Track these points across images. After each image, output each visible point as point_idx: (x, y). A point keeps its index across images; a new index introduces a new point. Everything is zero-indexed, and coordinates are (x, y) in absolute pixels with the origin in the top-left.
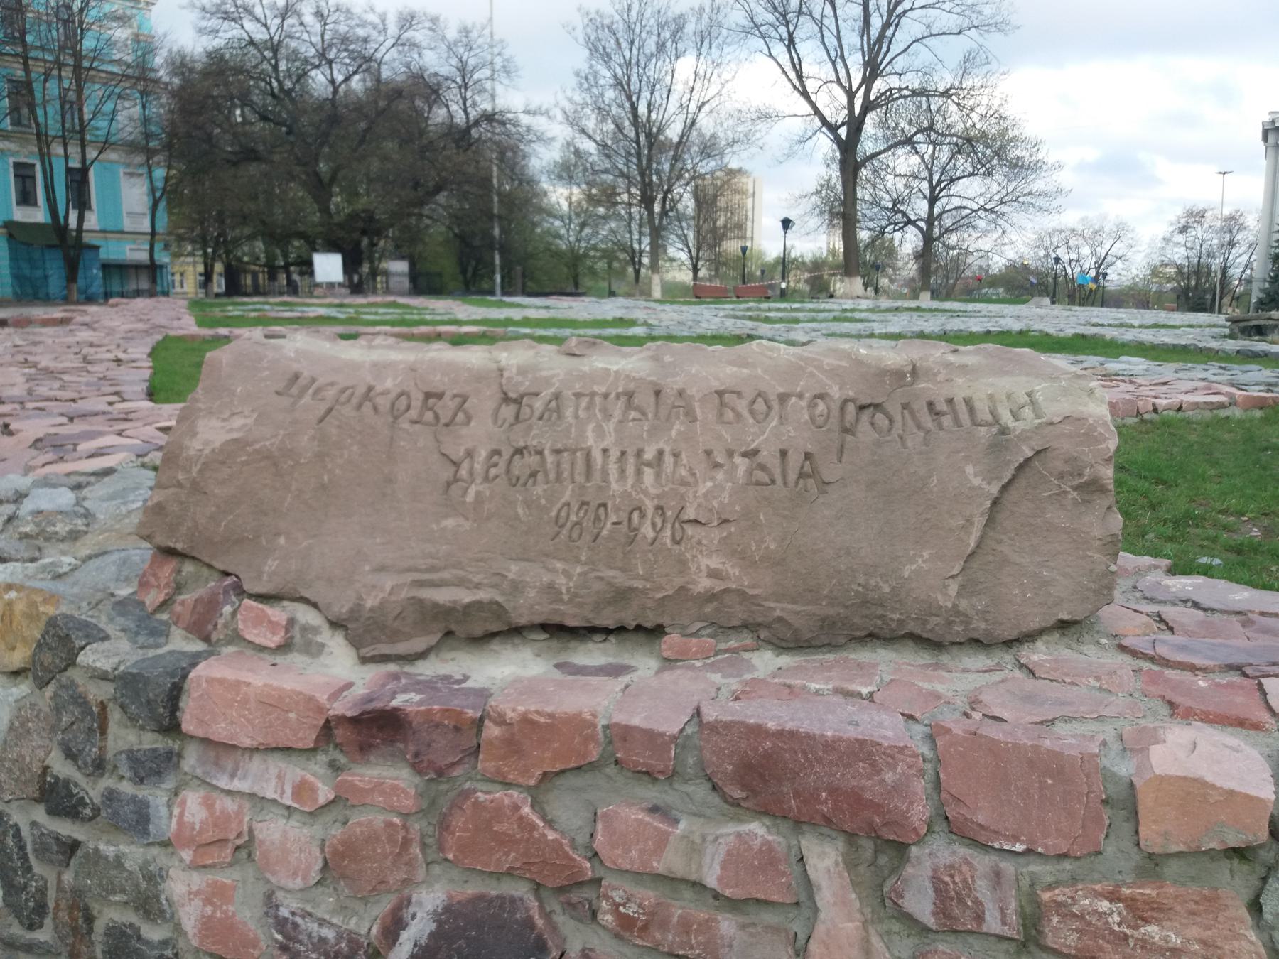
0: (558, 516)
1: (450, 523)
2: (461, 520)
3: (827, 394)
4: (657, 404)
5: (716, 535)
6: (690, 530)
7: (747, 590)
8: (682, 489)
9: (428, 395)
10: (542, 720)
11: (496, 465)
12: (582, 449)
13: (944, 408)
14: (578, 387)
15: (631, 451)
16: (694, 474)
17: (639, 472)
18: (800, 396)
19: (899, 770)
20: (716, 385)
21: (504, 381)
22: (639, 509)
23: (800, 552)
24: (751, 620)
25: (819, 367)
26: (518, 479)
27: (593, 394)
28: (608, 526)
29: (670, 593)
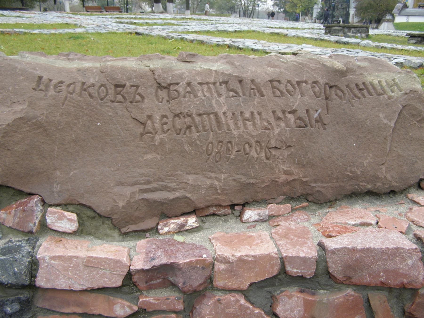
0: (207, 149)
1: (149, 156)
2: (155, 155)
3: (317, 81)
4: (242, 87)
5: (286, 153)
6: (274, 152)
7: (303, 179)
8: (267, 131)
9: (116, 86)
10: (250, 259)
11: (166, 123)
12: (212, 113)
13: (363, 87)
14: (199, 80)
15: (237, 113)
16: (270, 124)
17: (245, 125)
18: (306, 82)
19: (414, 259)
20: (268, 78)
21: (156, 77)
22: (248, 143)
23: (322, 159)
24: (304, 193)
25: (309, 68)
26: (180, 130)
27: (207, 83)
28: (234, 153)
29: (268, 184)
